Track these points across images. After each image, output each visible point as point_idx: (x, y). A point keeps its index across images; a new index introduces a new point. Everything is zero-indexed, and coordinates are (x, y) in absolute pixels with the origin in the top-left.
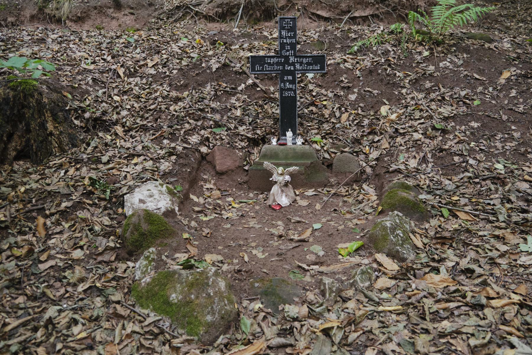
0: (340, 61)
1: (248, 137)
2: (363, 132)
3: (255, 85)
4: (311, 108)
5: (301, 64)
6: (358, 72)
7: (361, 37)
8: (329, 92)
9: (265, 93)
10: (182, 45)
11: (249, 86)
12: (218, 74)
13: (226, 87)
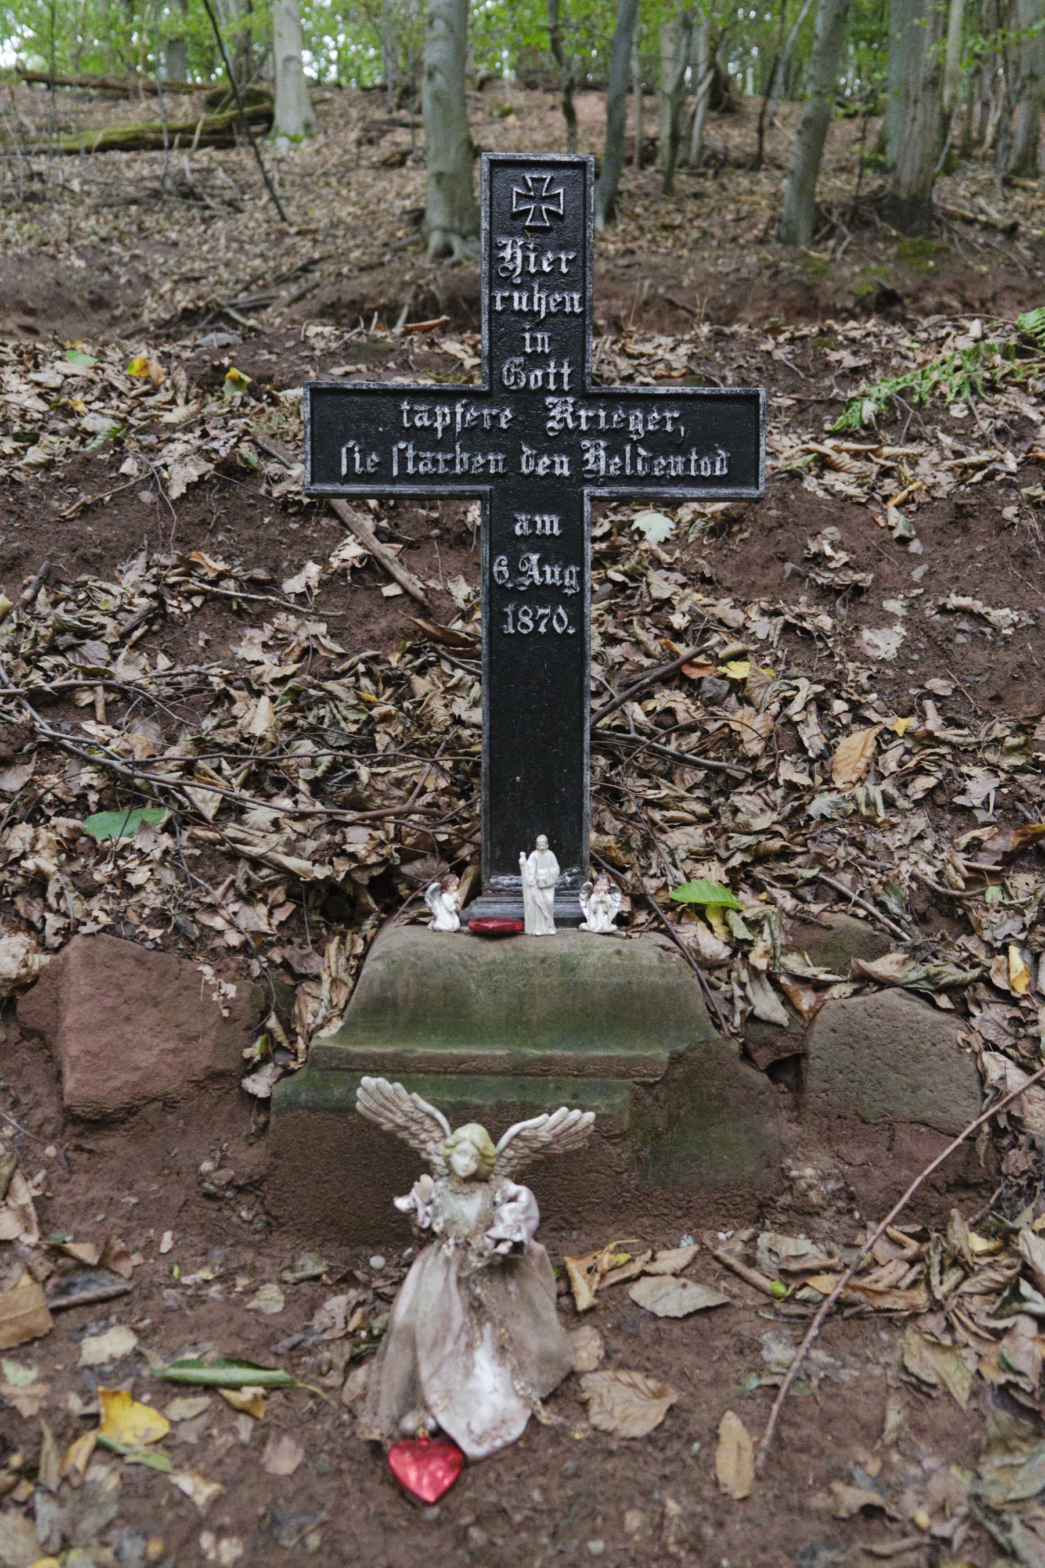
0: (798, 463)
1: (290, 876)
2: (975, 847)
3: (372, 569)
4: (665, 698)
5: (617, 439)
6: (895, 516)
7: (885, 367)
8: (753, 612)
9: (425, 611)
10: (56, 381)
11: (342, 574)
12: (194, 512)
13: (222, 576)
